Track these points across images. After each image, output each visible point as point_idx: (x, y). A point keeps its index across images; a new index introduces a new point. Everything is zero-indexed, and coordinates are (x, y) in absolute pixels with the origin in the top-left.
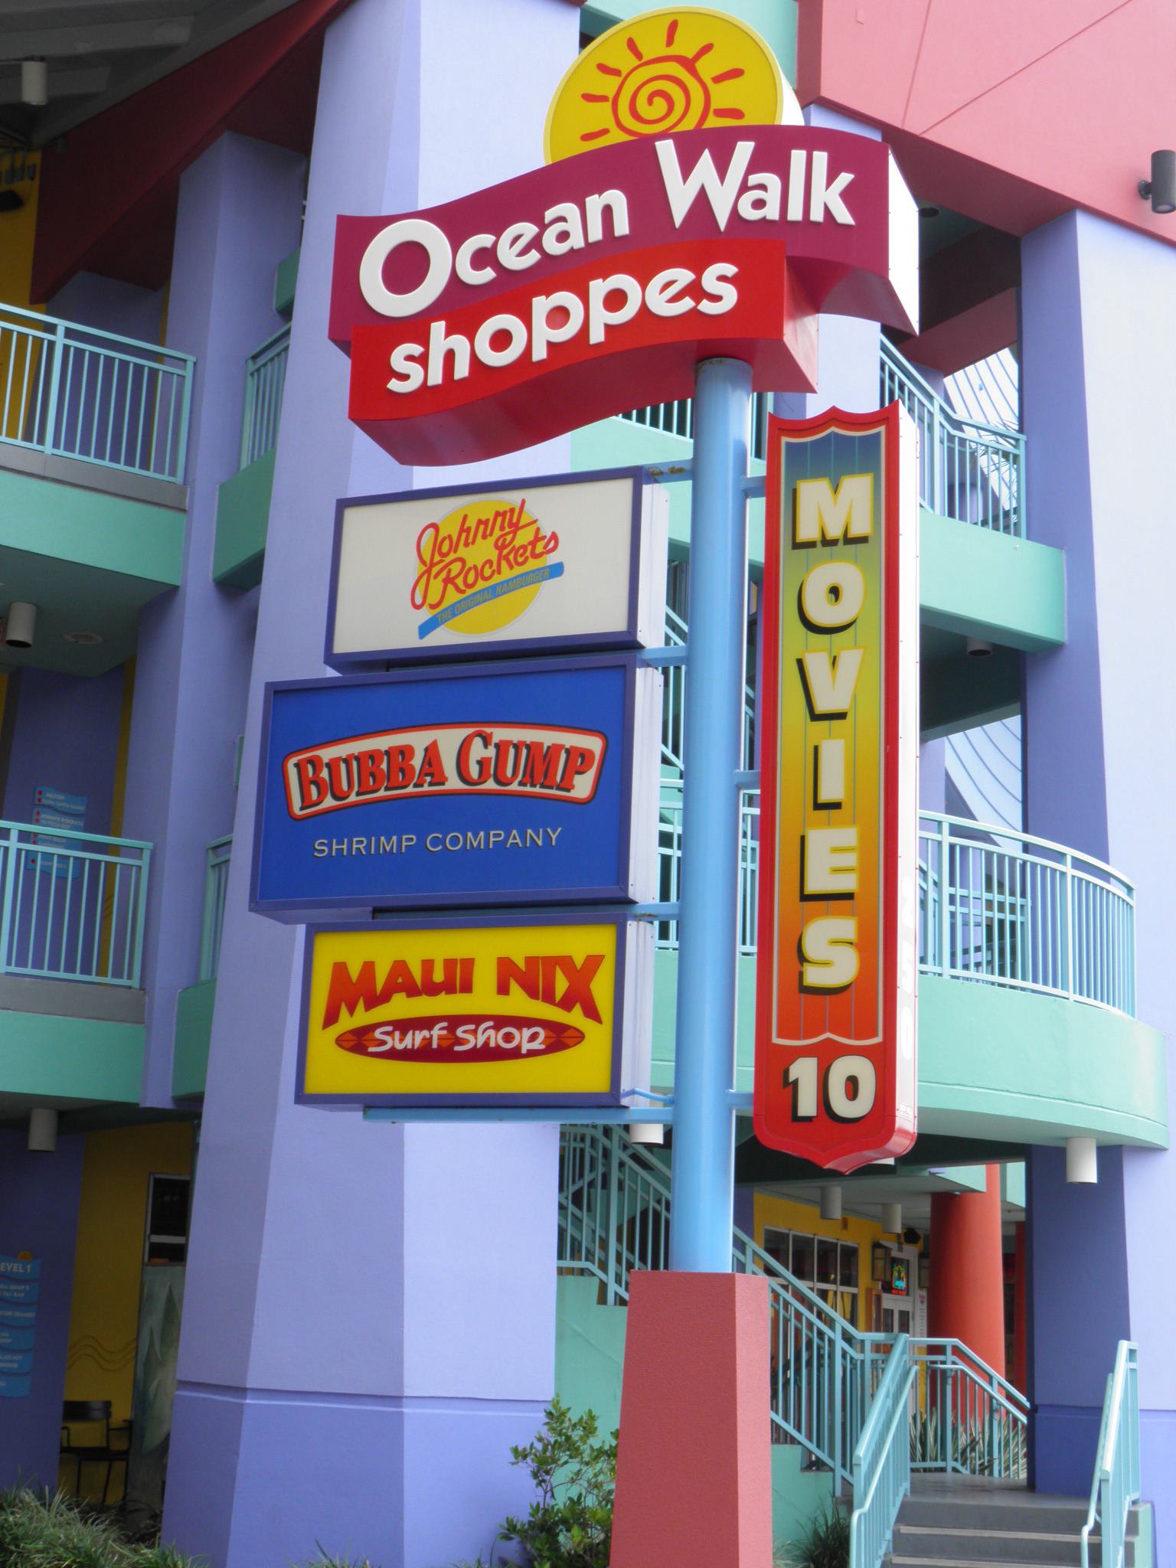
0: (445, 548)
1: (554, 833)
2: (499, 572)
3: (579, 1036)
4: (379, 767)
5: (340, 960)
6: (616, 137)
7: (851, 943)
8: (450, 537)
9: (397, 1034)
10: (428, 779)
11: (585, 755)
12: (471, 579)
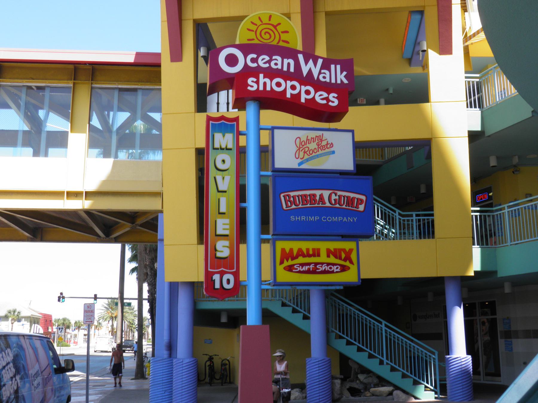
0: (303, 144)
2: (318, 151)
3: (349, 268)
6: (256, 42)
7: (228, 247)
8: (304, 141)
9: (301, 267)
10: (321, 203)
12: (311, 152)
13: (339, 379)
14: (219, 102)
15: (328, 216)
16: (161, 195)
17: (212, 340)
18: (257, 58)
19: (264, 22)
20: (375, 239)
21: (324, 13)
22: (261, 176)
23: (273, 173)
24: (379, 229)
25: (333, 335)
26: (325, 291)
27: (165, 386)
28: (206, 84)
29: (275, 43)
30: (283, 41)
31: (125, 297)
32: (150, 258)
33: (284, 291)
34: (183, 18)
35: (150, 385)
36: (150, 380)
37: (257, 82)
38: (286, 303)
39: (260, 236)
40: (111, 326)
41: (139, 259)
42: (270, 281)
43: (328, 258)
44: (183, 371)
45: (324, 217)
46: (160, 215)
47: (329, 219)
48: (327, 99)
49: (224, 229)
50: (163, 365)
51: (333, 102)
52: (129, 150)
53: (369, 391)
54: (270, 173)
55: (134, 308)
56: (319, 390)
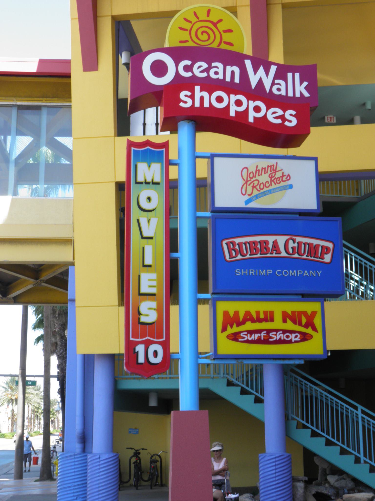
0: (251, 176)
1: (319, 272)
2: (271, 185)
3: (311, 337)
4: (257, 246)
5: (226, 310)
6: (190, 44)
7: (155, 309)
8: (253, 172)
9: (249, 335)
10: (275, 252)
11: (328, 248)
12: (262, 187)
13: (302, 482)
14: (146, 122)
15: (277, 270)
16: (72, 242)
17: (138, 429)
18: (192, 65)
19: (200, 19)
20: (348, 298)
21: (280, 6)
22: (197, 218)
23: (212, 214)
24: (354, 285)
25: (294, 423)
26: (283, 366)
27: (77, 490)
28: (126, 99)
29: (215, 45)
30: (226, 43)
31: (27, 373)
32: (60, 323)
33: (217, 366)
34: (98, 14)
35: (58, 488)
36: (58, 482)
37: (192, 97)
38: (232, 381)
39: (196, 295)
40: (11, 412)
41: (45, 325)
42: (209, 353)
43: (285, 324)
44: (101, 470)
45: (278, 270)
46: (70, 268)
47: (286, 273)
48: (282, 117)
49: (150, 286)
50: (75, 462)
51: (290, 121)
52: (32, 185)
53: (342, 498)
54: (208, 214)
55: (40, 388)
56: (276, 496)
